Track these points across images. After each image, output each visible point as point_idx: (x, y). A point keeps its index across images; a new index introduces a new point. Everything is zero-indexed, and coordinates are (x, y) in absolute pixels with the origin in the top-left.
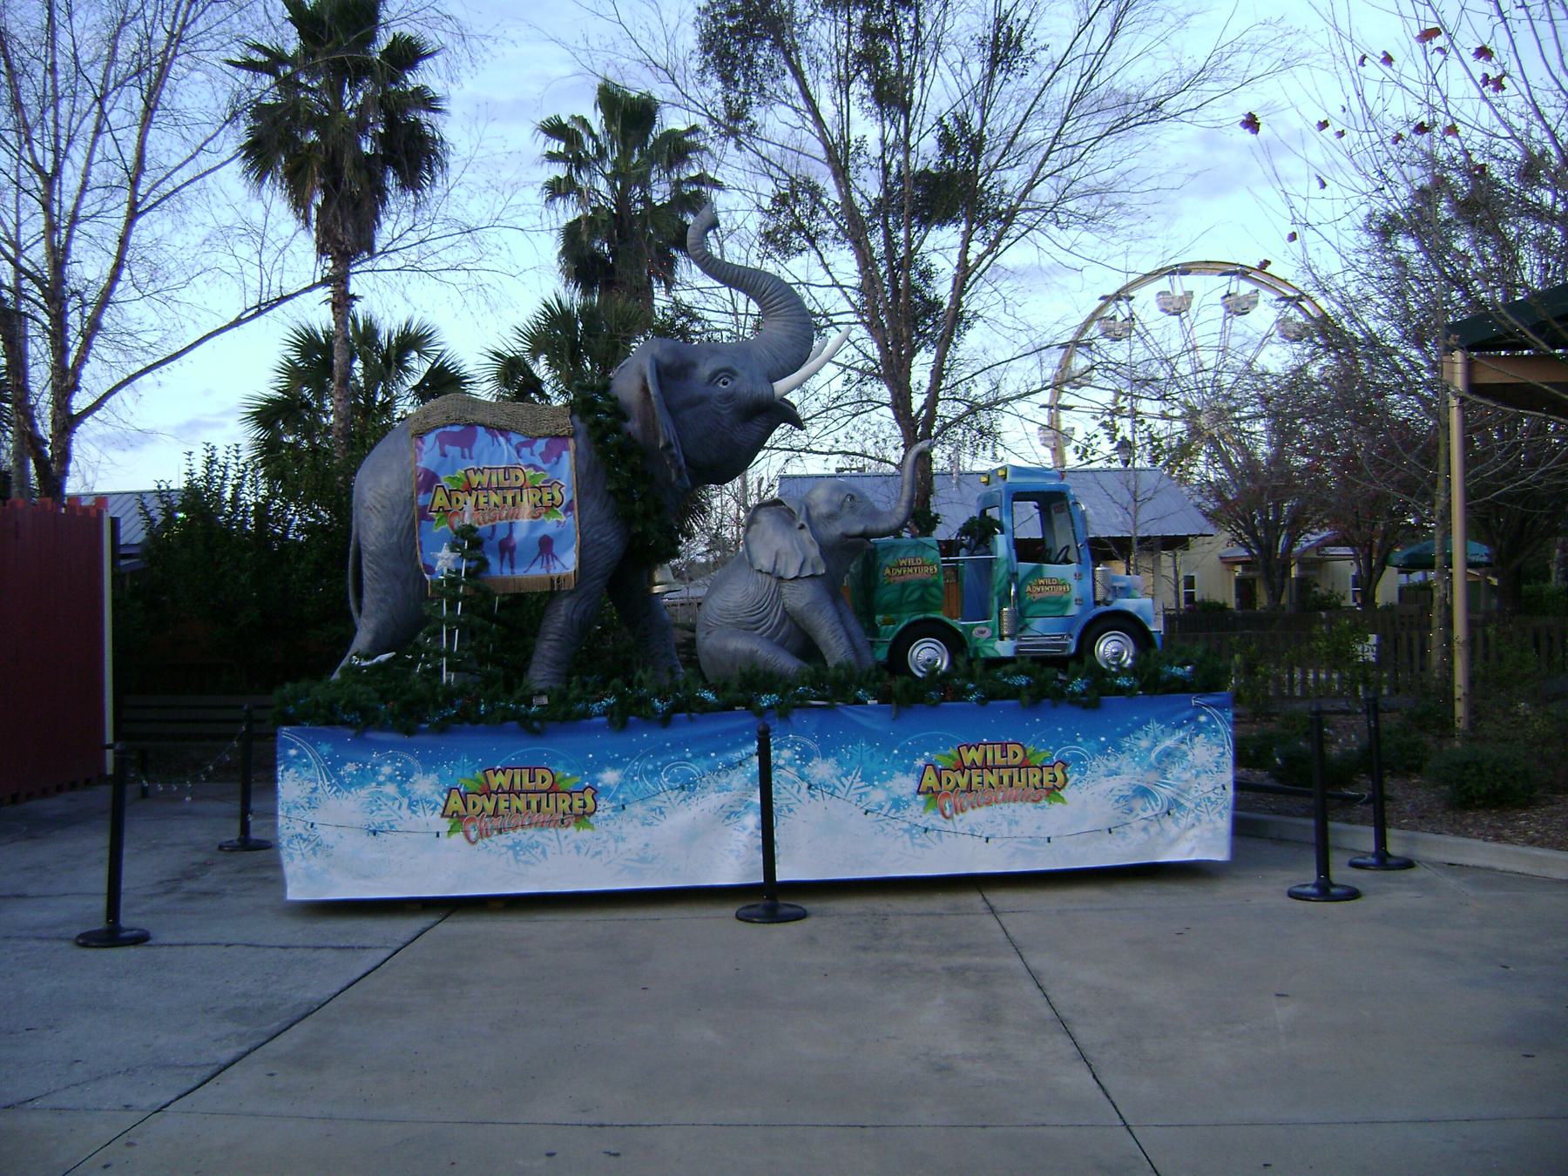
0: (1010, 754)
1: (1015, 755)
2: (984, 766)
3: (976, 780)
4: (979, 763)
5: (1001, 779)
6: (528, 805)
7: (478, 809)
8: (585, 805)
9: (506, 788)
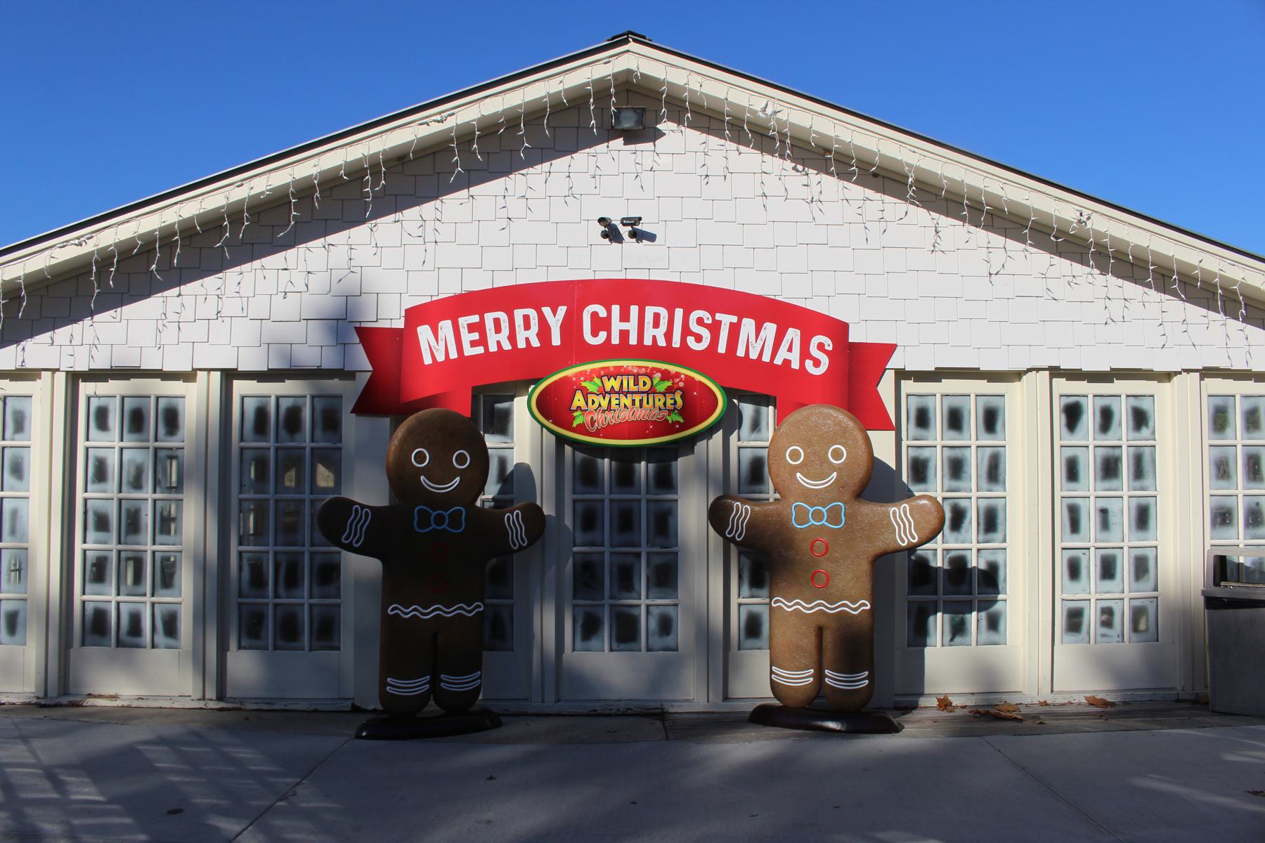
0: (641, 383)
1: (645, 384)
2: (621, 392)
3: (614, 402)
4: (617, 389)
5: (634, 401)
6: (634, 401)
7: (596, 405)
8: (675, 403)
9: (617, 389)
